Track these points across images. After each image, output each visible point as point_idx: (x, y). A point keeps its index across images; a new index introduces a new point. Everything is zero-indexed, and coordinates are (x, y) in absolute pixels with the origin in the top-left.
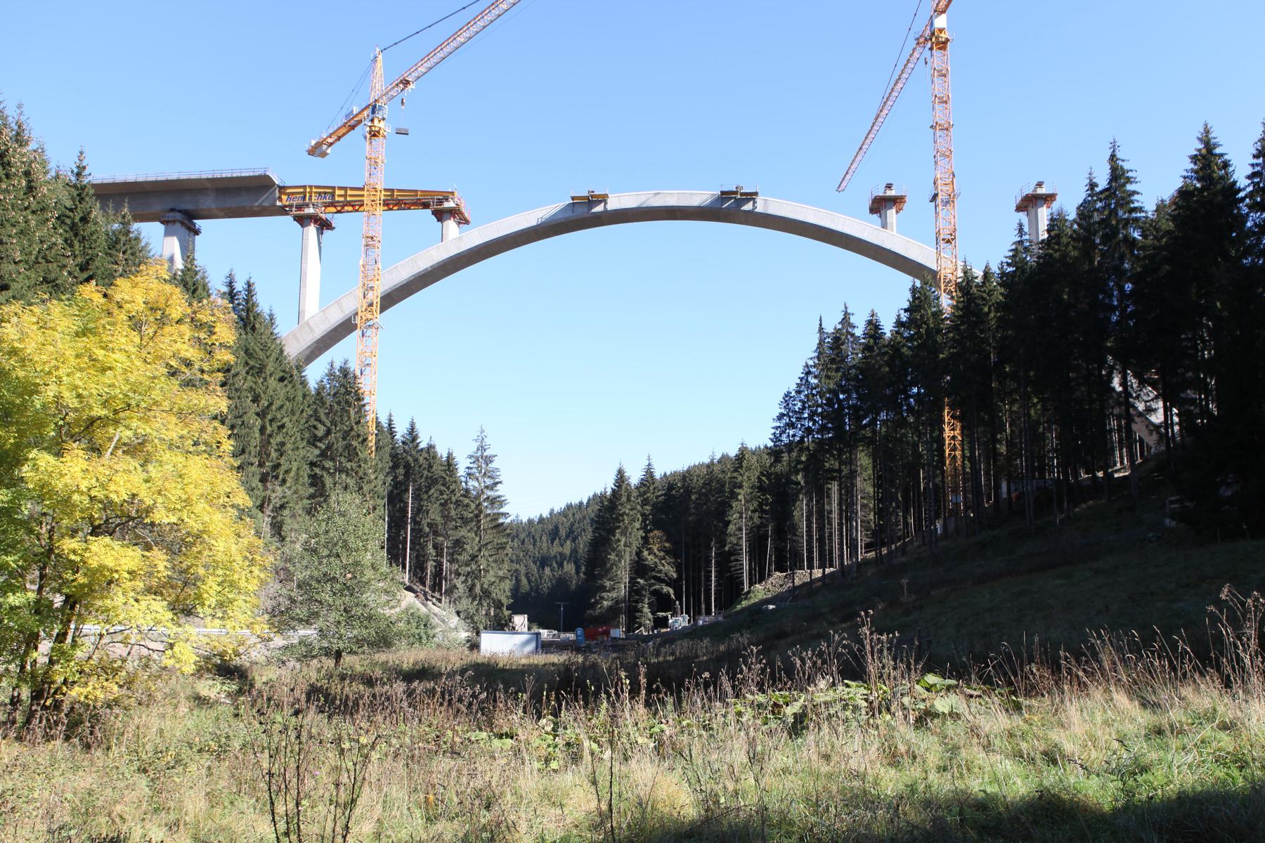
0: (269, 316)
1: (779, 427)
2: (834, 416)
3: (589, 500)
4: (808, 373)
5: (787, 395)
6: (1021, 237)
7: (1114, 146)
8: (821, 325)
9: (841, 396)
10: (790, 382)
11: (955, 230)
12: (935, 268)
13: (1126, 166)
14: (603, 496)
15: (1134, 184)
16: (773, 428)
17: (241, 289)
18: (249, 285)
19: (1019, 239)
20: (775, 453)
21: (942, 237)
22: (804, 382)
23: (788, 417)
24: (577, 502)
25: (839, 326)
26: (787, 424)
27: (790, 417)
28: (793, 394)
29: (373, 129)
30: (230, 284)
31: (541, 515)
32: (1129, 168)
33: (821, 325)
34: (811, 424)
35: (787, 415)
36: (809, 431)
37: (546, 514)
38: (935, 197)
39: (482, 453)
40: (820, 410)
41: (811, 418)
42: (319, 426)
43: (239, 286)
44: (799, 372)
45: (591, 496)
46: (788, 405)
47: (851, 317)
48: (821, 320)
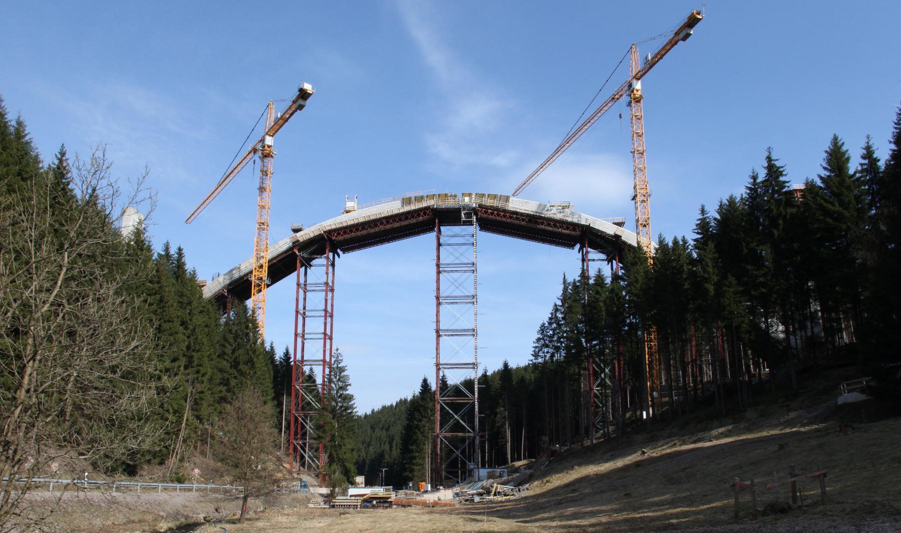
1: (538, 347)
3: (397, 403)
4: (556, 310)
5: (543, 325)
6: (703, 215)
7: (769, 150)
8: (564, 278)
10: (544, 316)
13: (778, 164)
14: (406, 400)
15: (784, 177)
17: (174, 253)
18: (180, 249)
21: (640, 222)
22: (553, 319)
23: (545, 338)
24: (389, 404)
26: (543, 345)
27: (544, 340)
29: (265, 152)
30: (167, 249)
31: (366, 413)
32: (781, 166)
33: (564, 278)
34: (559, 344)
35: (543, 339)
37: (369, 412)
38: (634, 198)
41: (558, 341)
42: (227, 345)
43: (173, 251)
44: (551, 308)
45: (398, 401)
46: (543, 332)
47: (570, 280)
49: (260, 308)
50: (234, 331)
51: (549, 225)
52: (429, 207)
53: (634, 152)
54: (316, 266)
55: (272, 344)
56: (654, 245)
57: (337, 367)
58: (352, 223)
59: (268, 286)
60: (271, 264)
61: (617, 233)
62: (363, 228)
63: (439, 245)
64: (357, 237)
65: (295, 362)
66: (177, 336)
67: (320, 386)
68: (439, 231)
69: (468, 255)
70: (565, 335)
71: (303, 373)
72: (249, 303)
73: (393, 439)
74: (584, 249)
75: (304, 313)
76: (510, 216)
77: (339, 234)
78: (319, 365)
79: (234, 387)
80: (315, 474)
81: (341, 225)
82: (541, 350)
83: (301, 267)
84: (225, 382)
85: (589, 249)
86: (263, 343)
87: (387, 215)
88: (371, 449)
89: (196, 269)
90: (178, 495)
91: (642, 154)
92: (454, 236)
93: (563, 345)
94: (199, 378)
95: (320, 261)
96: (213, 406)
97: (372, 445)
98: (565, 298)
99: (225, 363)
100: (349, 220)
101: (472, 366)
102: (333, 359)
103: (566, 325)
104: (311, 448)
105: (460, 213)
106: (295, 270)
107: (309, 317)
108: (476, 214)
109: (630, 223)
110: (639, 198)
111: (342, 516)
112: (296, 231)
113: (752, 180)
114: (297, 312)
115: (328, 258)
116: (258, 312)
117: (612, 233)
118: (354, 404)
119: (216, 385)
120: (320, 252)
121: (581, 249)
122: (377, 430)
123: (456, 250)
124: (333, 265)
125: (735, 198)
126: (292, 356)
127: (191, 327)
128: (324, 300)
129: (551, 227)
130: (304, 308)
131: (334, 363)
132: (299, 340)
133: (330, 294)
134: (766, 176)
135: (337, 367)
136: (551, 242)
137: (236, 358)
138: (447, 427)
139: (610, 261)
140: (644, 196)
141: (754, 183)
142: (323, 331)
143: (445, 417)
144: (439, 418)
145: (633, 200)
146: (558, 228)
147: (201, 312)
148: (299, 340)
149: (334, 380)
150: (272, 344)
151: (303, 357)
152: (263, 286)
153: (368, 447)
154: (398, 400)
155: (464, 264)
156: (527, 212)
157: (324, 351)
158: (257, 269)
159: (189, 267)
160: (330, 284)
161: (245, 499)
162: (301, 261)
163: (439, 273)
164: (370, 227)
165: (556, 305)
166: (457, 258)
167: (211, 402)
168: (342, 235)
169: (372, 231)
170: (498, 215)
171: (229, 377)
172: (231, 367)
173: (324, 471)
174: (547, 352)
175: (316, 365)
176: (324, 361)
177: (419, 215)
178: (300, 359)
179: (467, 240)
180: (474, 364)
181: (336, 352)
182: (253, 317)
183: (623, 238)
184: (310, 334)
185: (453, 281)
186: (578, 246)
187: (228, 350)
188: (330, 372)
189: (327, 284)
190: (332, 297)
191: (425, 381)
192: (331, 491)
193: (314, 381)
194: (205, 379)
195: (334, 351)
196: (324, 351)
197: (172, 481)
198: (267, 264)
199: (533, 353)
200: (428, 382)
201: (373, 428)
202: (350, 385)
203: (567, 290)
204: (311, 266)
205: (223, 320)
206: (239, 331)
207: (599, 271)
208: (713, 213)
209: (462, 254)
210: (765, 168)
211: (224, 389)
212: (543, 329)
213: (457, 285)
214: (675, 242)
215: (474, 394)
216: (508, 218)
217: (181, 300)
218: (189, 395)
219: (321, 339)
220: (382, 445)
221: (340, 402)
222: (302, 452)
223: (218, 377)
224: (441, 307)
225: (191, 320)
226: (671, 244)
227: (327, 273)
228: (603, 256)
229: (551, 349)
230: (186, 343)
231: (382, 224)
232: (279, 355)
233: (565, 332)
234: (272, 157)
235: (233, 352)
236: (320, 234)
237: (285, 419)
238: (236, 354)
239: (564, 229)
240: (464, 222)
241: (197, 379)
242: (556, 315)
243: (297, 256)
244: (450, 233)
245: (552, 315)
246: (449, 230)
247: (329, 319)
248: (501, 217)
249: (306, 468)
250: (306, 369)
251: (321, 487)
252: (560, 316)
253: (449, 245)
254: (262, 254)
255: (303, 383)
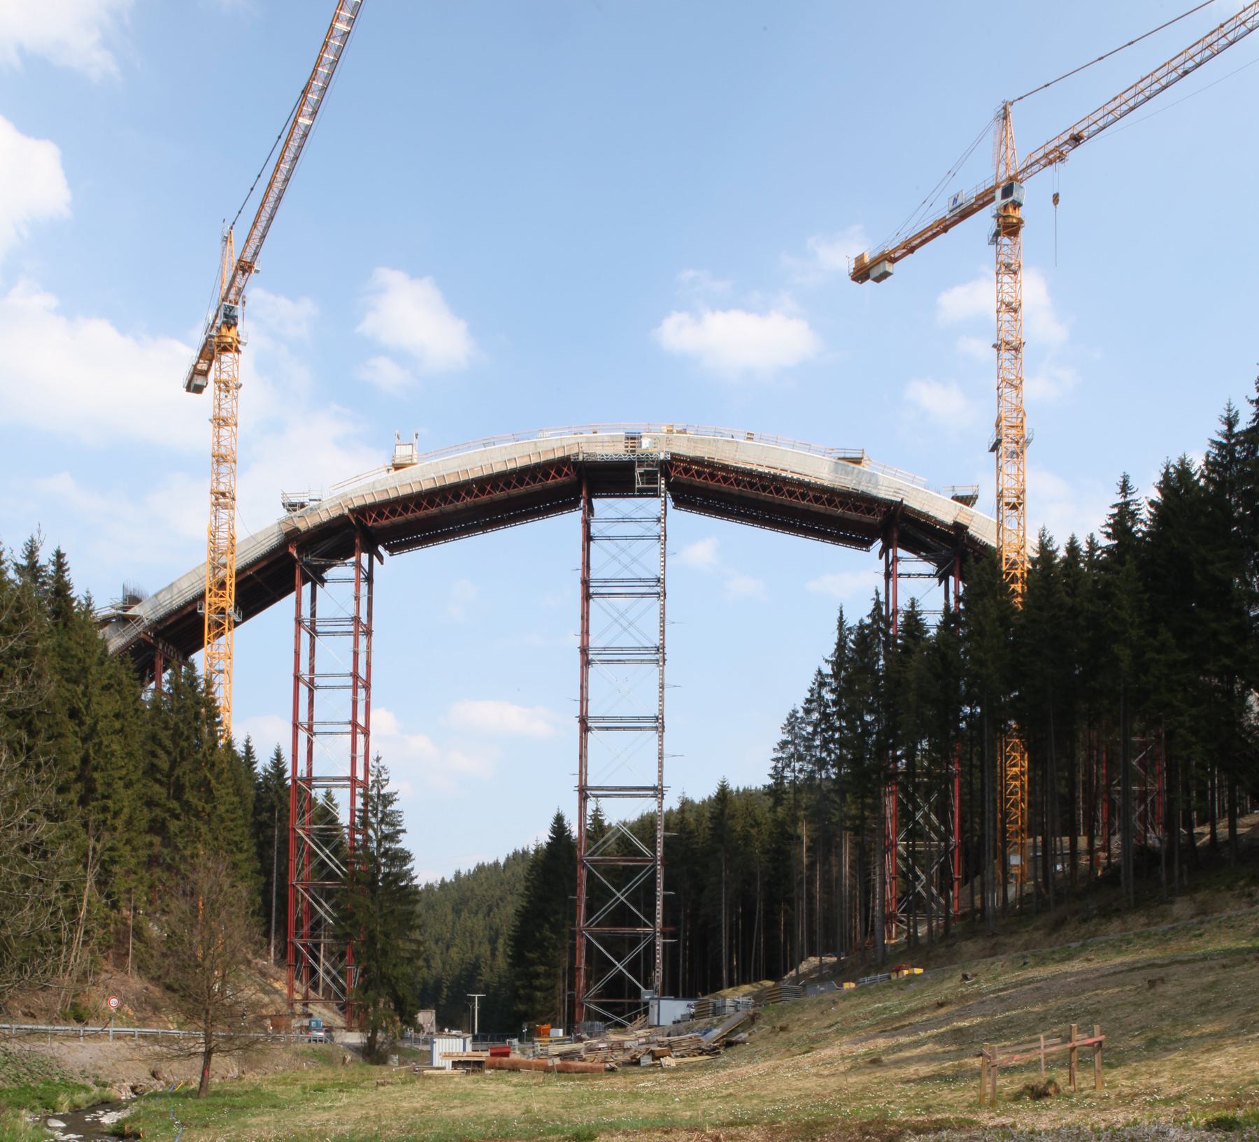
0: (86, 599)
1: (781, 758)
2: (854, 742)
4: (822, 685)
6: (1125, 497)
8: (841, 617)
9: (868, 718)
10: (797, 698)
11: (1023, 492)
12: (994, 545)
14: (525, 853)
16: (773, 760)
18: (59, 555)
19: (1122, 500)
20: (775, 792)
22: (814, 700)
24: (491, 862)
25: (868, 621)
26: (792, 756)
28: (801, 714)
30: (32, 553)
31: (443, 879)
33: (841, 617)
34: (824, 755)
35: (792, 742)
36: (821, 763)
37: (449, 878)
38: (995, 448)
39: (379, 791)
40: (837, 735)
41: (824, 745)
42: (160, 752)
43: (45, 558)
44: (809, 680)
46: (793, 728)
47: (852, 621)
48: (841, 612)
49: (221, 671)
50: (171, 724)
51: (817, 499)
52: (568, 458)
53: (1000, 345)
54: (334, 581)
55: (248, 741)
56: (1032, 551)
57: (379, 795)
58: (407, 491)
59: (236, 624)
60: (240, 578)
61: (960, 520)
62: (432, 503)
63: (588, 538)
64: (418, 520)
65: (294, 781)
66: (62, 741)
67: (346, 831)
68: (590, 510)
69: (647, 561)
70: (837, 735)
71: (312, 802)
72: (199, 659)
73: (497, 934)
74: (891, 551)
75: (312, 681)
76: (736, 480)
77: (380, 515)
78: (344, 786)
79: (176, 835)
80: (337, 1004)
81: (384, 497)
82: (789, 766)
83: (304, 583)
84: (157, 827)
85: (901, 552)
86: (229, 745)
87: (480, 474)
88: (454, 952)
89: (92, 593)
90: (84, 1047)
91: (1016, 349)
92: (623, 520)
93: (833, 756)
94: (109, 822)
95: (341, 573)
96: (135, 873)
97: (456, 945)
98: (840, 661)
99: (157, 787)
100: (402, 486)
101: (652, 792)
102: (371, 778)
103: (841, 715)
104: (330, 954)
105: (633, 470)
106: (294, 590)
107: (322, 687)
108: (666, 475)
109: (987, 498)
110: (1007, 446)
111: (381, 1088)
112: (292, 507)
113: (1225, 428)
114: (297, 679)
115: (358, 565)
116: (218, 679)
117: (949, 520)
118: (412, 869)
119: (140, 833)
120: (340, 552)
121: (884, 551)
122: (464, 914)
123: (623, 550)
124: (369, 579)
125: (1191, 463)
126: (289, 767)
127: (88, 721)
128: (352, 654)
129: (823, 503)
130: (312, 670)
131: (373, 786)
132: (303, 735)
133: (363, 640)
134: (1254, 420)
135: (379, 795)
136: (822, 535)
137: (178, 777)
138: (600, 914)
139: (943, 577)
140: (1017, 443)
141: (1229, 435)
142: (350, 718)
143: (598, 895)
144: (584, 897)
145: (992, 450)
146: (836, 506)
147: (106, 688)
148: (303, 735)
149: (373, 820)
150: (248, 741)
151: (310, 771)
152: (226, 626)
153: (448, 948)
154: (511, 854)
155: (641, 580)
156: (772, 471)
157: (354, 760)
158: (214, 589)
159: (77, 592)
160: (364, 620)
161: (208, 1055)
162: (303, 572)
163: (587, 597)
164: (445, 500)
165: (820, 672)
166: (626, 567)
167: (131, 866)
168: (387, 518)
169: (448, 508)
170: (713, 476)
171: (167, 815)
172: (168, 798)
173: (356, 1000)
174: (801, 770)
175: (337, 786)
176: (353, 779)
177: (546, 476)
178: (305, 775)
179: (648, 529)
180: (654, 788)
181: (375, 764)
182: (208, 693)
183: (971, 531)
184: (324, 723)
185: (616, 615)
186: (878, 544)
187: (163, 763)
188: (365, 804)
189: (356, 620)
190: (369, 647)
191: (559, 819)
192: (368, 1038)
193: (334, 820)
194: (119, 823)
195: (372, 761)
196: (354, 760)
197: (66, 1019)
198: (233, 580)
199: (772, 772)
200: (565, 822)
201: (457, 911)
202: (404, 831)
203: (845, 643)
204: (323, 581)
205: (147, 696)
206: (181, 725)
207: (913, 605)
208: (1147, 494)
209: (634, 560)
210: (1252, 402)
211: (157, 840)
212: (792, 722)
213: (625, 624)
214: (1073, 548)
215: (655, 852)
216: (732, 484)
217: (66, 665)
218: (90, 853)
219: (347, 733)
220: (476, 946)
221: (384, 864)
222: (311, 961)
223: (143, 822)
224: (592, 670)
225: (87, 707)
226: (1062, 553)
227: (357, 598)
228: (930, 568)
229: (809, 762)
230: (82, 753)
231: (470, 493)
232: (263, 762)
233: (840, 729)
234: (238, 351)
235: (172, 768)
236: (342, 516)
237: (277, 894)
238: (178, 772)
239: (849, 509)
240: (640, 490)
241: (104, 822)
242: (819, 693)
243: (294, 561)
244: (611, 514)
245: (812, 695)
246: (610, 506)
247: (362, 693)
248: (718, 481)
249: (321, 993)
250: (319, 794)
251: (349, 1029)
252: (829, 696)
253: (609, 538)
254: (223, 560)
255: (311, 822)
